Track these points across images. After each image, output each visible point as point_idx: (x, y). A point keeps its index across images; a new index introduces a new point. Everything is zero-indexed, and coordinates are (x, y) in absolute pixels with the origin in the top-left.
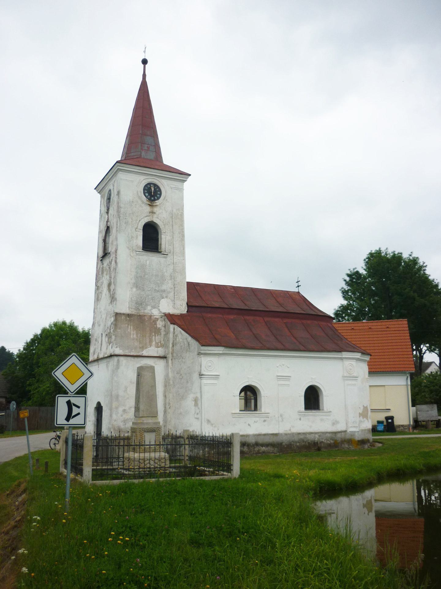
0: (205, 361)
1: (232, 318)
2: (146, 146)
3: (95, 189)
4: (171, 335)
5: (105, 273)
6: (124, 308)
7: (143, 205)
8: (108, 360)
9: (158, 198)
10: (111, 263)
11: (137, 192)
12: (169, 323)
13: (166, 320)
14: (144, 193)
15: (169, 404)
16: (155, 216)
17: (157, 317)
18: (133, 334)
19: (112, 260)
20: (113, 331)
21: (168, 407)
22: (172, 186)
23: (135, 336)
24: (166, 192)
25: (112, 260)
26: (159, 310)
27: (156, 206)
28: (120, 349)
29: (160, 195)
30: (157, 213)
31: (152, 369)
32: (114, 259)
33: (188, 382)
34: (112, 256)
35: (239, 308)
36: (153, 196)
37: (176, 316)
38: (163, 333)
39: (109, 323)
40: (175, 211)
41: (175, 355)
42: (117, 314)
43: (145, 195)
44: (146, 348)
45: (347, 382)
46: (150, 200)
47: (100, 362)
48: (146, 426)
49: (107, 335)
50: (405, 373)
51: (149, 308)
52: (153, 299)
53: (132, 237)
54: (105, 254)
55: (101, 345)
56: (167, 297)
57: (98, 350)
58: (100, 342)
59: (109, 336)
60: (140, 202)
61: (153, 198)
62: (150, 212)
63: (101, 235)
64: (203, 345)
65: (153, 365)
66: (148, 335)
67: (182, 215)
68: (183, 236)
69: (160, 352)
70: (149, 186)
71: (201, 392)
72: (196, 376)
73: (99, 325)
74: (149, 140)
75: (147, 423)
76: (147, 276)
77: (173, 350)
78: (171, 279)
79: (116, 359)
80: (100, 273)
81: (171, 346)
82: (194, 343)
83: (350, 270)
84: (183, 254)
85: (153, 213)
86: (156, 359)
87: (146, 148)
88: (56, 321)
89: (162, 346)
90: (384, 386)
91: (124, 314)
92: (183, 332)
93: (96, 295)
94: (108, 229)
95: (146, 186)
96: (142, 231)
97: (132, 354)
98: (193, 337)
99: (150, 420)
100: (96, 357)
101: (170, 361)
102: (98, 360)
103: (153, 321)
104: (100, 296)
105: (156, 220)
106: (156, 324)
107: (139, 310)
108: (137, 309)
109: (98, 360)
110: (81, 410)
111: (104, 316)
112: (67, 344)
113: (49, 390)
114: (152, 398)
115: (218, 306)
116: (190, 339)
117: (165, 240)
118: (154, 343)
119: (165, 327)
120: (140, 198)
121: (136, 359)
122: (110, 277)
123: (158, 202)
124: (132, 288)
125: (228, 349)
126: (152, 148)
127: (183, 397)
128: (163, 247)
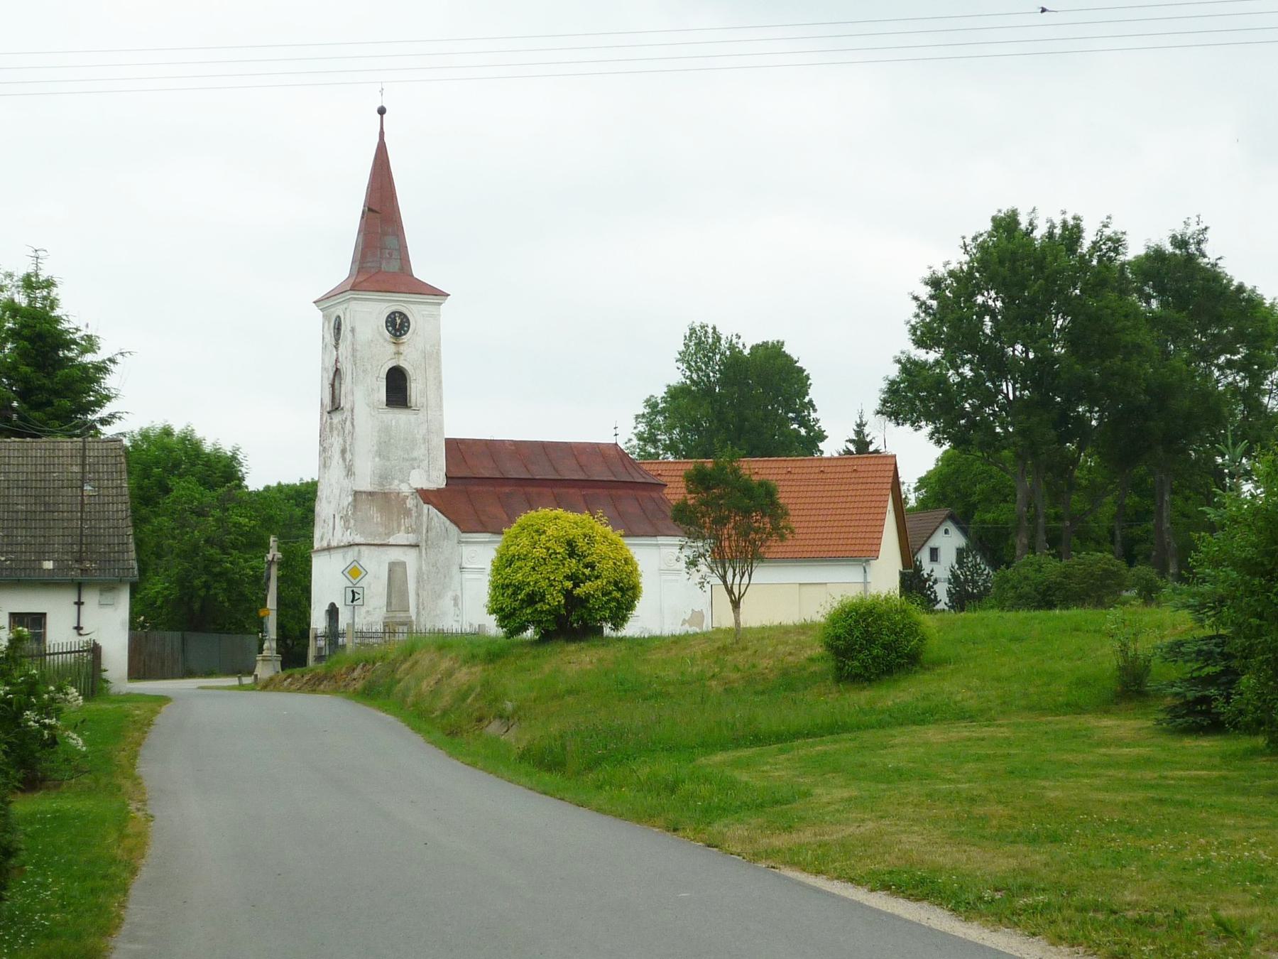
0: (467, 551)
1: (507, 491)
2: (387, 251)
3: (315, 302)
4: (425, 518)
5: (335, 433)
6: (365, 484)
7: (386, 344)
8: (346, 549)
9: (406, 333)
10: (345, 421)
11: (378, 327)
12: (422, 502)
13: (418, 497)
14: (387, 327)
15: (423, 604)
16: (402, 358)
17: (407, 494)
18: (377, 517)
19: (346, 418)
20: (352, 514)
21: (421, 607)
22: (424, 313)
23: (379, 519)
24: (416, 322)
25: (346, 418)
26: (409, 484)
27: (403, 343)
28: (361, 537)
29: (408, 327)
30: (405, 353)
31: (403, 564)
32: (349, 418)
33: (445, 577)
34: (347, 414)
35: (517, 477)
36: (398, 330)
37: (431, 491)
38: (414, 514)
39: (346, 504)
40: (428, 347)
41: (429, 542)
42: (356, 494)
43: (388, 330)
44: (393, 534)
45: (664, 577)
46: (395, 336)
47: (332, 552)
48: (398, 620)
49: (341, 517)
50: (860, 561)
51: (396, 482)
52: (401, 470)
53: (373, 389)
54: (335, 407)
55: (334, 529)
56: (419, 467)
57: (328, 536)
58: (331, 525)
59: (345, 519)
60: (382, 341)
61: (398, 334)
62: (395, 354)
63: (326, 375)
64: (463, 532)
65: (402, 559)
66: (395, 518)
67: (438, 353)
68: (440, 382)
69: (411, 538)
70: (393, 316)
71: (462, 589)
72: (455, 569)
73: (330, 502)
74: (391, 241)
75: (400, 617)
76: (392, 441)
77: (427, 537)
78: (424, 443)
79: (356, 548)
80: (328, 429)
81: (424, 531)
82: (453, 529)
83: (931, 268)
84: (440, 407)
85: (398, 353)
86: (406, 548)
87: (388, 256)
88: (145, 426)
89: (414, 531)
90: (826, 584)
91: (365, 492)
92: (439, 513)
93: (322, 458)
94: (337, 372)
95: (389, 316)
96: (385, 380)
97: (375, 542)
98: (451, 521)
99: (402, 614)
100: (325, 544)
101: (424, 551)
102: (329, 549)
103: (400, 499)
104: (328, 462)
105: (403, 364)
106: (405, 503)
107: (384, 486)
108: (381, 484)
109: (329, 549)
110: (361, 596)
111: (337, 492)
112: (189, 488)
113: (171, 594)
114: (404, 594)
115: (488, 476)
116: (448, 522)
117: (415, 389)
118: (403, 528)
119: (417, 506)
120: (381, 334)
121: (381, 549)
122: (345, 442)
123: (405, 338)
124: (373, 458)
125: (494, 536)
126: (395, 255)
127: (439, 596)
128: (413, 399)
